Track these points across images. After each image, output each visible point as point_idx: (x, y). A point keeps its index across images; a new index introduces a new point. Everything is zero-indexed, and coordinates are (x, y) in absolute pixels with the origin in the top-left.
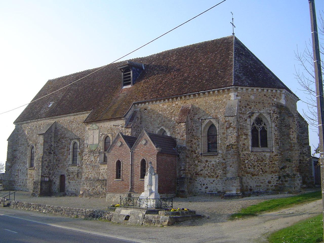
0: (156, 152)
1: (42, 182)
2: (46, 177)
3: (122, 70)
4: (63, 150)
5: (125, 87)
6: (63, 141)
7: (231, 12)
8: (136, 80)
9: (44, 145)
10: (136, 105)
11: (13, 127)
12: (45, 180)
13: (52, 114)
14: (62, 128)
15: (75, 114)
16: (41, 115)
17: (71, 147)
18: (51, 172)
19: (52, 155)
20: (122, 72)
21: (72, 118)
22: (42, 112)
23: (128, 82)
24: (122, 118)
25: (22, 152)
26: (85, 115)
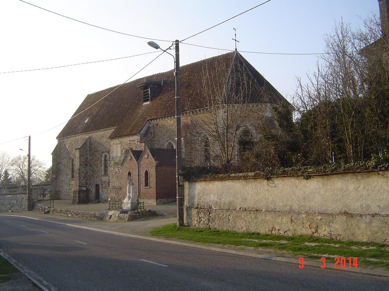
0: (155, 164)
1: (80, 191)
2: (83, 186)
3: (142, 88)
4: (96, 162)
5: (145, 104)
6: (97, 154)
7: (234, 29)
8: (154, 97)
9: (80, 158)
10: (150, 121)
11: (56, 142)
12: (83, 189)
13: (88, 129)
14: (95, 142)
15: (104, 129)
16: (78, 130)
17: (103, 159)
18: (88, 182)
19: (88, 167)
20: (142, 89)
21: (103, 133)
22: (79, 127)
23: (147, 99)
24: (137, 134)
25: (65, 164)
26: (110, 131)
